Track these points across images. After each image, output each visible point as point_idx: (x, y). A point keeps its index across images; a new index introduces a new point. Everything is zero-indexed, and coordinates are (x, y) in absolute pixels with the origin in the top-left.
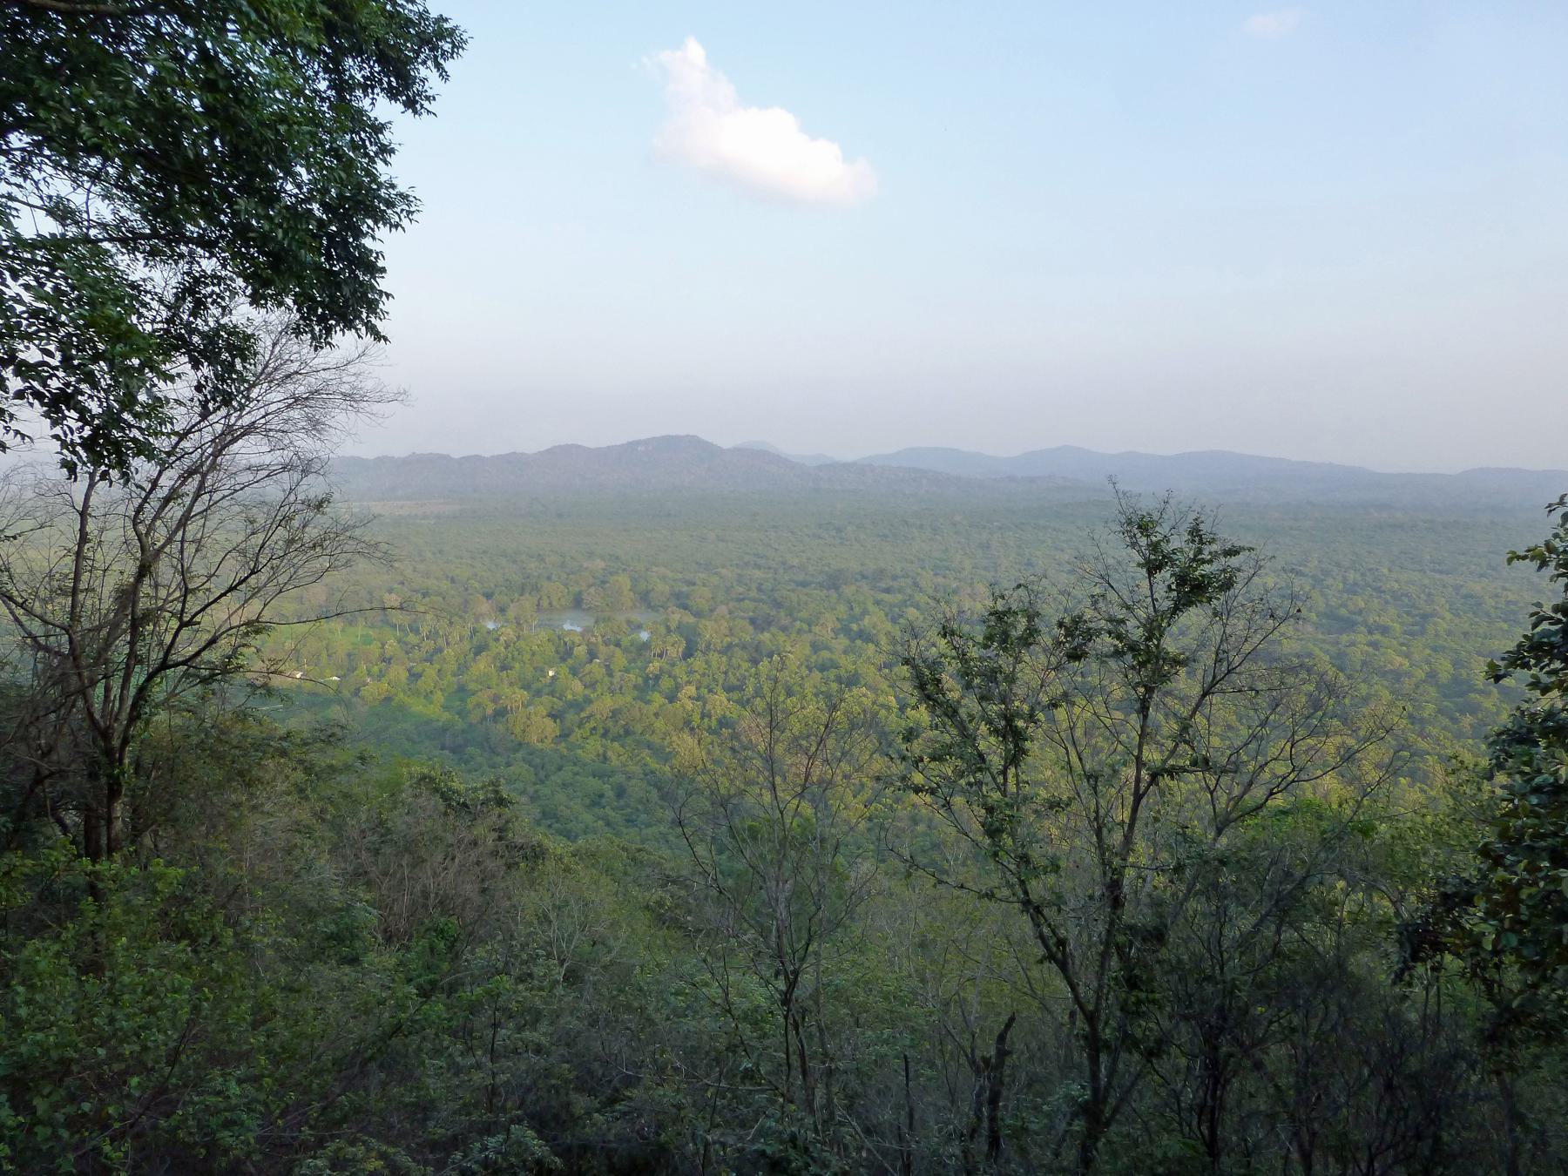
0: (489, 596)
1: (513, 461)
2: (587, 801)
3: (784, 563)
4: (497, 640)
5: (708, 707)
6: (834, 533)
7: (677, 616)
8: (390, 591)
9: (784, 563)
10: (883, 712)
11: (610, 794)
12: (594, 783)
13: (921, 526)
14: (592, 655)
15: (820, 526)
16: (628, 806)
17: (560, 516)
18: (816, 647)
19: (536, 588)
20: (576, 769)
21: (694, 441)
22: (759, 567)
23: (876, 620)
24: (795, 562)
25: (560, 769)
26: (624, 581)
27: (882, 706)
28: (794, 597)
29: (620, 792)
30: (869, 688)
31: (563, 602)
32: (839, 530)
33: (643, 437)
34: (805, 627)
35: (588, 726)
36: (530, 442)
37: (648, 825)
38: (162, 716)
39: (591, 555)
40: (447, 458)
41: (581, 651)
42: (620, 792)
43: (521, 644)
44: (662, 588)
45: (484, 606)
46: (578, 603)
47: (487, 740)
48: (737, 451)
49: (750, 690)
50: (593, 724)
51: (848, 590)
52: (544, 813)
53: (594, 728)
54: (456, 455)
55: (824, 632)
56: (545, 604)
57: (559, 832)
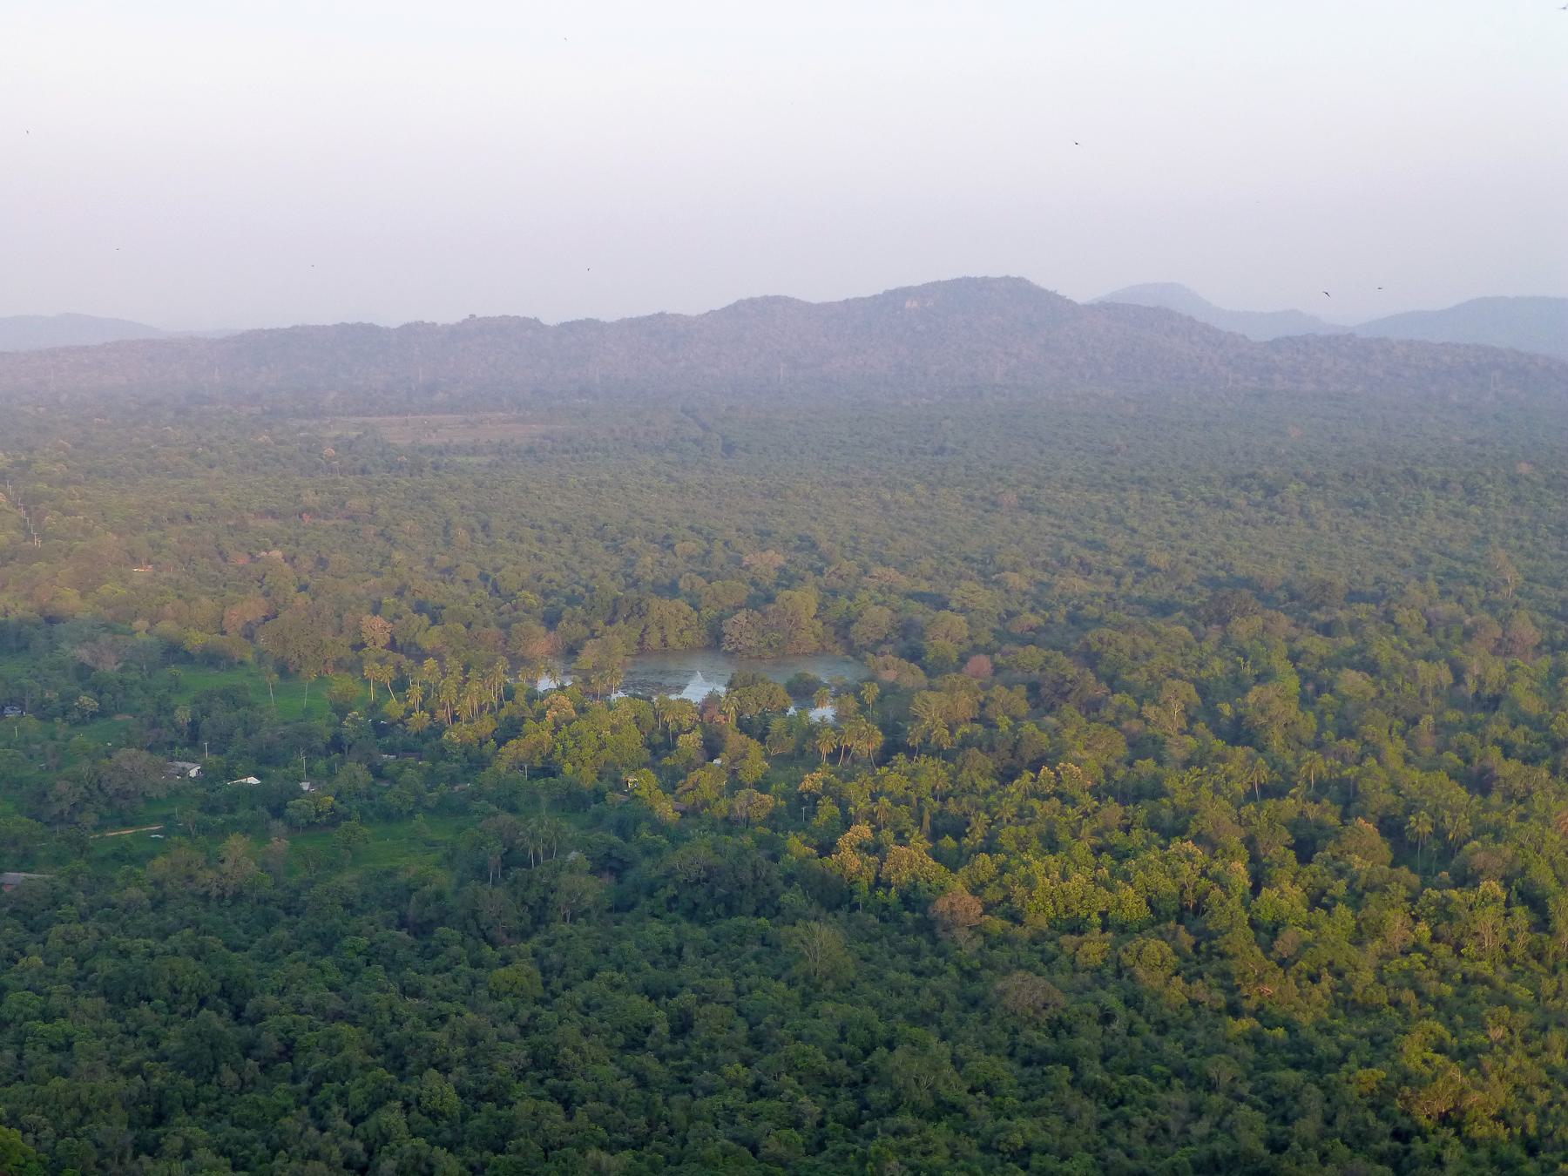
0: (551, 621)
1: (658, 330)
2: (620, 1039)
3: (1138, 562)
4: (541, 716)
5: (887, 868)
6: (1258, 496)
7: (894, 670)
8: (376, 609)
9: (1138, 562)
10: (1217, 892)
11: (663, 1028)
12: (639, 1005)
13: (1445, 485)
14: (712, 748)
15: (1234, 481)
16: (686, 1051)
17: (729, 449)
18: (1140, 747)
19: (638, 610)
20: (618, 977)
21: (1018, 290)
22: (1085, 568)
23: (1276, 701)
24: (1162, 559)
25: (591, 975)
26: (804, 599)
27: (1216, 879)
28: (1124, 641)
29: (682, 1026)
30: (1198, 839)
31: (688, 636)
32: (1270, 491)
33: (916, 281)
34: (1131, 704)
35: (663, 895)
36: (695, 293)
37: (709, 1092)
38: (1082, 1039)
39: (764, 537)
40: (533, 325)
41: (690, 742)
42: (682, 1026)
43: (582, 725)
44: (878, 617)
45: (540, 643)
46: (715, 641)
47: (474, 914)
48: (1108, 309)
49: (977, 836)
50: (671, 890)
51: (1242, 629)
52: (536, 1061)
53: (675, 898)
54: (551, 318)
55: (1167, 717)
56: (654, 639)
57: (555, 1094)
